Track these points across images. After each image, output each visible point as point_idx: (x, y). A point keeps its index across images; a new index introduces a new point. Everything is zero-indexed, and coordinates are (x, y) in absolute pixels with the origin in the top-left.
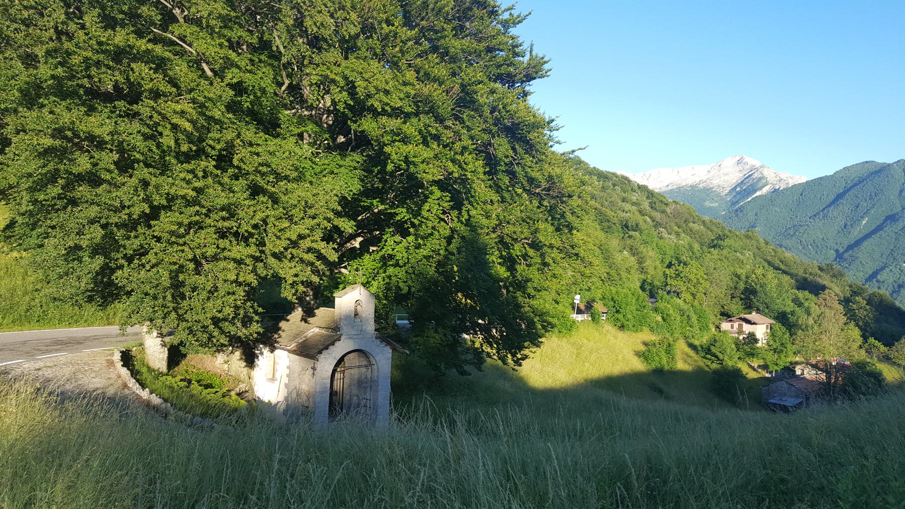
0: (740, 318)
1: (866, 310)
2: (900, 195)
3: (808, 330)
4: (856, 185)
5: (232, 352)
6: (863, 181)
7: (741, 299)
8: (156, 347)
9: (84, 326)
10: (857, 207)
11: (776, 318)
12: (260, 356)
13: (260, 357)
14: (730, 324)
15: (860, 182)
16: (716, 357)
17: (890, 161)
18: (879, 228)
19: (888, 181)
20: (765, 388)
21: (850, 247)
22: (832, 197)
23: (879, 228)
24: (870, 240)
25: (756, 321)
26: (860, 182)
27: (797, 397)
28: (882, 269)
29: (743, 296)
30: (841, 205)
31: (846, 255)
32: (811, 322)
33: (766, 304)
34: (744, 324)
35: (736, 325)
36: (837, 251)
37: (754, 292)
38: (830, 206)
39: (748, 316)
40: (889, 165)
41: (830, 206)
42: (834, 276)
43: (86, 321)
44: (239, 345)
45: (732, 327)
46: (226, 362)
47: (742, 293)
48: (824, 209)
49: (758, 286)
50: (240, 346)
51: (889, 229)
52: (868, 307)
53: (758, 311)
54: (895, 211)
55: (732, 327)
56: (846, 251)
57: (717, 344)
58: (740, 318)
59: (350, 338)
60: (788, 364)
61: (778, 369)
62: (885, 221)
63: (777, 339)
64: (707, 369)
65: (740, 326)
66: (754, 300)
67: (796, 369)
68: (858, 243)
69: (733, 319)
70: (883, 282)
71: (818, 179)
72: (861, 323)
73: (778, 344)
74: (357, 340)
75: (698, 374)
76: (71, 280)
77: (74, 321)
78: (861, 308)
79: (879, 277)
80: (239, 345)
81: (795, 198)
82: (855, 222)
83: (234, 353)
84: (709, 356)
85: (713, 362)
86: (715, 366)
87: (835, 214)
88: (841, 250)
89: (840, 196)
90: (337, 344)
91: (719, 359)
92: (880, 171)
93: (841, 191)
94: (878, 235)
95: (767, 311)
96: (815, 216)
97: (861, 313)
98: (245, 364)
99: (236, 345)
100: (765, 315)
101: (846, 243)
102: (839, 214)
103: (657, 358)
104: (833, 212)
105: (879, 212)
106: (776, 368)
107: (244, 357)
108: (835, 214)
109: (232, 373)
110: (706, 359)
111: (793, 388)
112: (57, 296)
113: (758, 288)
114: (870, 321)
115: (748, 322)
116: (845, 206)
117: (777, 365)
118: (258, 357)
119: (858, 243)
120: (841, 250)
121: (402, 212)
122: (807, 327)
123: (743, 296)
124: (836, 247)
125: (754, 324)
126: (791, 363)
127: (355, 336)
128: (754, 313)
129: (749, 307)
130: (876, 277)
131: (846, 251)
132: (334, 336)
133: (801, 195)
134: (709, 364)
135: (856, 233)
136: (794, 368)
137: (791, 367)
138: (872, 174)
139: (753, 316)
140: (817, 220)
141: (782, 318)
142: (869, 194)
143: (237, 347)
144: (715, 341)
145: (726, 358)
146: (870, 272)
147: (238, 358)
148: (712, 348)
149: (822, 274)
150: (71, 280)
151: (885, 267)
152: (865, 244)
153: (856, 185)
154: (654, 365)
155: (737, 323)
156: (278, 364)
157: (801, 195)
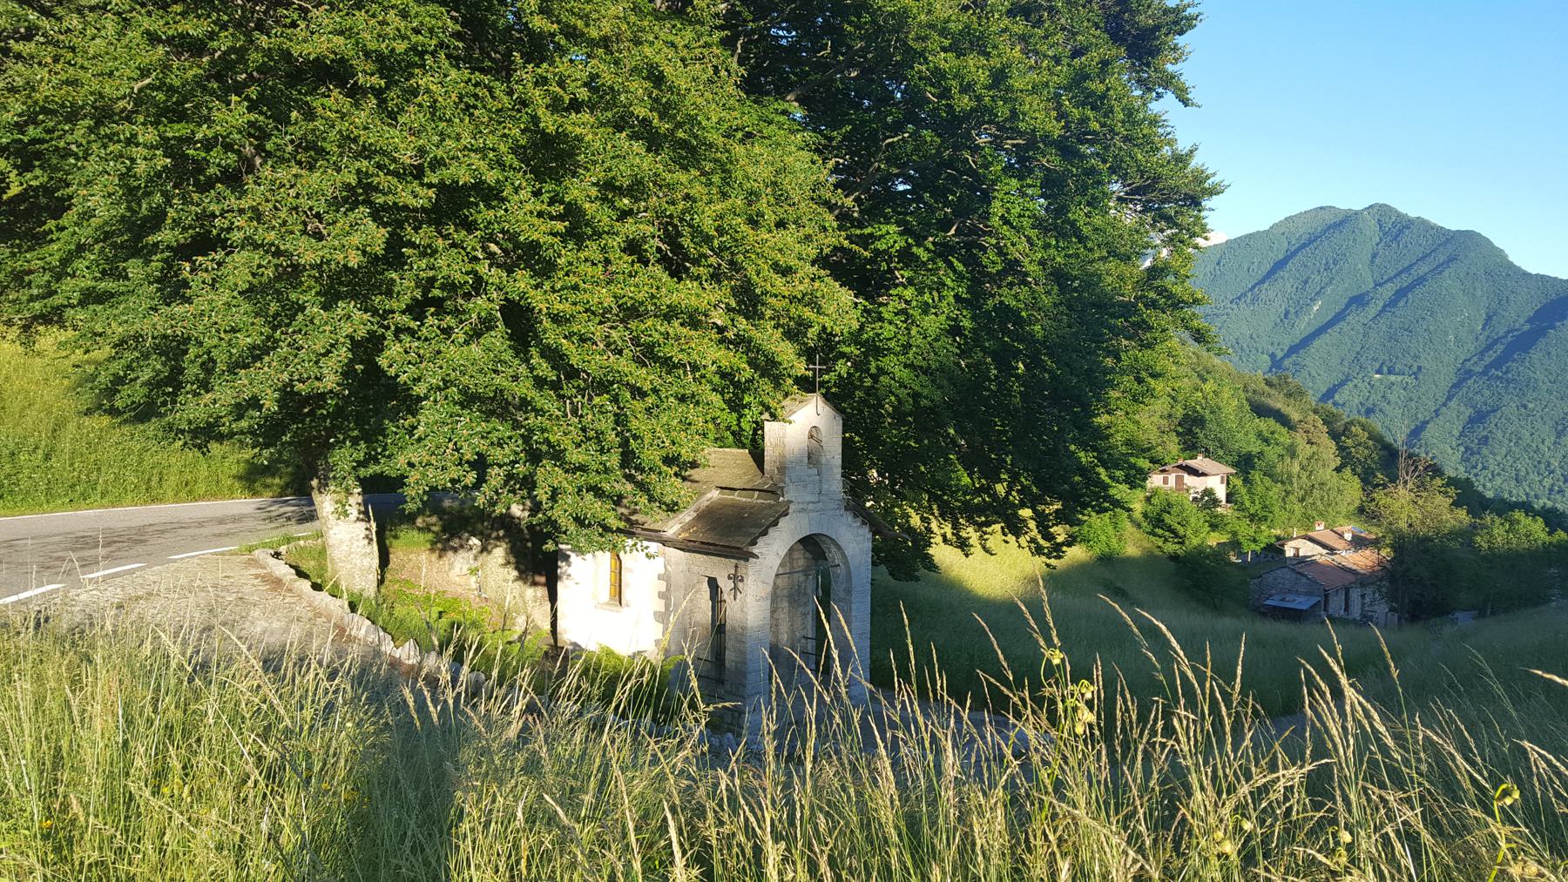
0: (1180, 467)
1: (1367, 448)
2: (1372, 262)
3: (1291, 483)
4: (1303, 246)
5: (484, 549)
6: (1315, 240)
7: (1178, 434)
8: (356, 543)
9: (103, 506)
10: (1306, 282)
11: (1233, 465)
12: (573, 555)
13: (573, 557)
14: (1161, 477)
15: (1311, 242)
16: (1173, 531)
17: (1358, 206)
18: (1339, 318)
19: (1355, 240)
20: (1256, 581)
21: (1293, 350)
22: (1267, 267)
23: (1339, 318)
24: (1325, 338)
25: (1206, 470)
26: (1311, 242)
27: (1309, 594)
28: (1342, 384)
29: (1180, 429)
30: (1280, 281)
31: (1286, 363)
32: (1296, 468)
33: (1220, 441)
34: (1186, 476)
35: (1172, 478)
36: (1273, 356)
37: (1200, 421)
38: (1262, 282)
39: (1191, 463)
40: (1356, 213)
41: (1262, 282)
42: (1289, 395)
43: (103, 495)
44: (501, 533)
45: (1165, 481)
46: (474, 571)
47: (1180, 424)
48: (1254, 287)
49: (1207, 412)
50: (504, 536)
51: (1355, 319)
52: (1371, 443)
53: (1207, 453)
54: (1364, 289)
55: (1165, 481)
56: (1288, 355)
57: (1174, 510)
58: (1180, 467)
59: (803, 510)
60: (1273, 540)
61: (1258, 548)
62: (1348, 306)
63: (1256, 498)
64: (1157, 552)
65: (1179, 480)
66: (1201, 435)
67: (1286, 548)
68: (1306, 342)
69: (1167, 468)
70: (1344, 405)
71: (1246, 236)
72: (1359, 470)
73: (1258, 506)
74: (815, 514)
75: (1149, 562)
76: (266, 369)
77: (151, 492)
78: (1360, 444)
79: (1337, 397)
80: (501, 533)
81: (1208, 269)
82: (1301, 308)
83: (489, 552)
84: (1160, 531)
85: (1166, 540)
86: (1171, 547)
87: (1271, 294)
88: (1280, 354)
89: (1280, 265)
90: (783, 522)
91: (1176, 535)
92: (1342, 223)
93: (1281, 256)
94: (1337, 328)
95: (1221, 452)
96: (1239, 298)
97: (1361, 453)
98: (515, 573)
99: (494, 535)
100: (1218, 459)
101: (1287, 342)
102: (1277, 296)
103: (1103, 538)
104: (1268, 291)
105: (1339, 293)
106: (1253, 546)
107: (512, 560)
108: (1271, 294)
109: (489, 594)
110: (1155, 535)
111: (1304, 580)
112: (1453, 266)
113: (1208, 415)
114: (1373, 466)
115: (1194, 472)
116: (1287, 280)
117: (1255, 541)
118: (566, 558)
119: (1306, 342)
120: (1280, 354)
121: (888, 233)
122: (1290, 476)
123: (1180, 429)
124: (1271, 350)
125: (1204, 474)
126: (1278, 538)
127: (811, 506)
128: (1200, 457)
129: (1191, 446)
130: (1333, 397)
131: (1288, 355)
132: (770, 506)
133: (1218, 264)
134: (1160, 544)
135: (1303, 326)
136: (1283, 545)
137: (1277, 544)
138: (1329, 228)
139: (1199, 462)
140: (1243, 305)
141: (1244, 464)
142: (1324, 262)
143: (498, 538)
144: (1169, 505)
145: (1189, 533)
146: (1324, 389)
147: (502, 561)
148: (1166, 517)
149: (1272, 392)
150: (266, 369)
151: (1347, 380)
152: (1317, 343)
153: (1303, 246)
154: (1097, 551)
155: (1174, 475)
156: (631, 571)
157: (1218, 264)
